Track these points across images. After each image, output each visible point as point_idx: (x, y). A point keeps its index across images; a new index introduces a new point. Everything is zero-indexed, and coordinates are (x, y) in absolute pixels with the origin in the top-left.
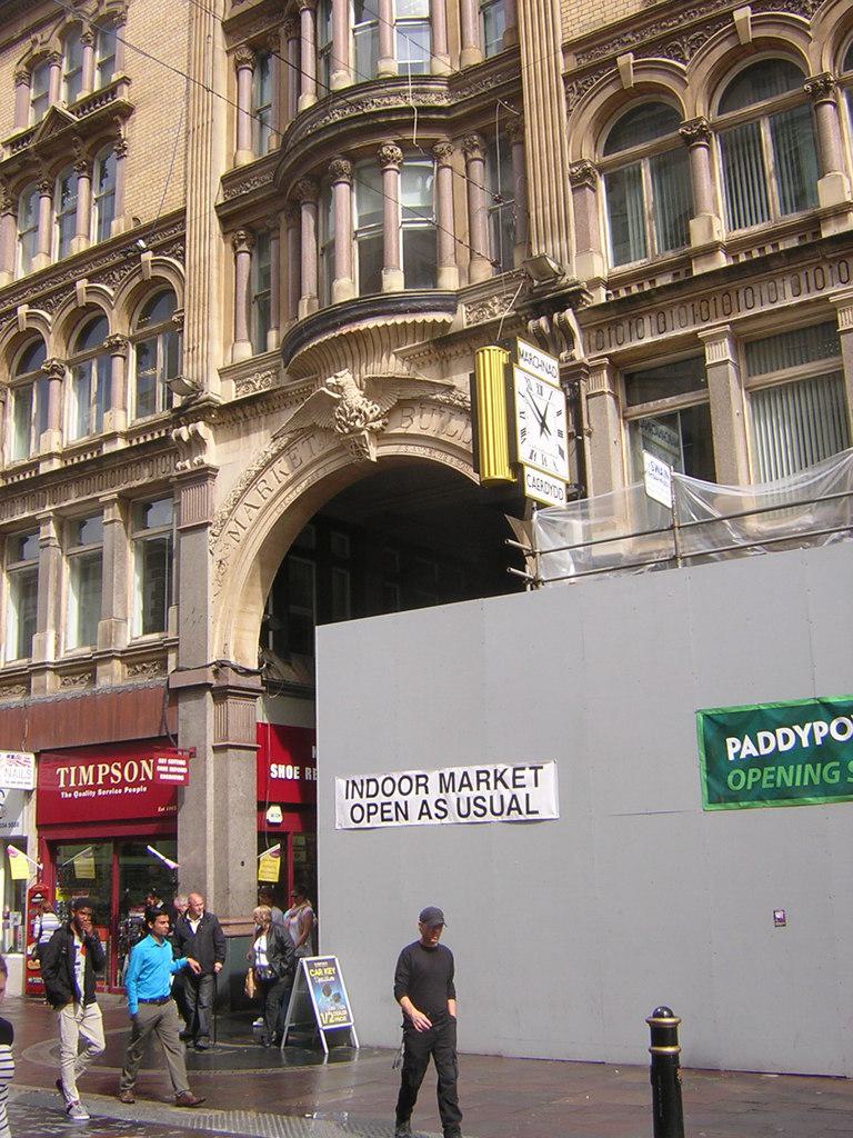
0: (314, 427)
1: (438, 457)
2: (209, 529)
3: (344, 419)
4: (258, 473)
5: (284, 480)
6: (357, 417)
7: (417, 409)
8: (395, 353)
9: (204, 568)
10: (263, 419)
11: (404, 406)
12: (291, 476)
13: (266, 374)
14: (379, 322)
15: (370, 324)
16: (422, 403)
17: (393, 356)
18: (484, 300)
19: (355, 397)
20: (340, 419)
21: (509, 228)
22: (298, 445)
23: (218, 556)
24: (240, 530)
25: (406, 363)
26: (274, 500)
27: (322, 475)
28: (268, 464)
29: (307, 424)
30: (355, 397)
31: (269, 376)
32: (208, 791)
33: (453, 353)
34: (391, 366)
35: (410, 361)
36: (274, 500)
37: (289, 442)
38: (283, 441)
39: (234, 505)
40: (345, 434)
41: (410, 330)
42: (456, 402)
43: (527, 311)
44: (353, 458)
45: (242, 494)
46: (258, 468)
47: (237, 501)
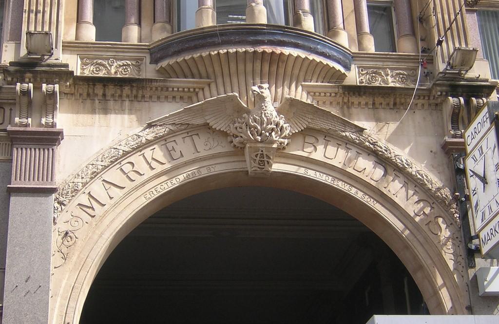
0: (207, 126)
1: (341, 185)
2: (54, 196)
3: (259, 128)
4: (126, 154)
5: (159, 168)
6: (273, 130)
7: (321, 139)
8: (302, 85)
9: (45, 237)
10: (127, 103)
11: (309, 134)
12: (168, 166)
13: (124, 62)
14: (303, 54)
15: (287, 51)
16: (328, 136)
17: (300, 88)
18: (379, 68)
19: (270, 109)
20: (256, 128)
21: (421, 20)
22: (179, 139)
23: (62, 227)
24: (95, 205)
25: (309, 96)
26: (143, 184)
27: (205, 173)
28: (139, 148)
29: (199, 121)
30: (270, 109)
31: (128, 65)
32: (471, 228)
33: (356, 102)
34: (299, 94)
35: (308, 93)
36: (143, 184)
37: (168, 134)
38: (161, 131)
39: (92, 178)
40: (256, 141)
41: (318, 70)
42: (367, 144)
43: (444, 88)
44: (250, 165)
45: (103, 170)
46: (127, 149)
47: (95, 175)
